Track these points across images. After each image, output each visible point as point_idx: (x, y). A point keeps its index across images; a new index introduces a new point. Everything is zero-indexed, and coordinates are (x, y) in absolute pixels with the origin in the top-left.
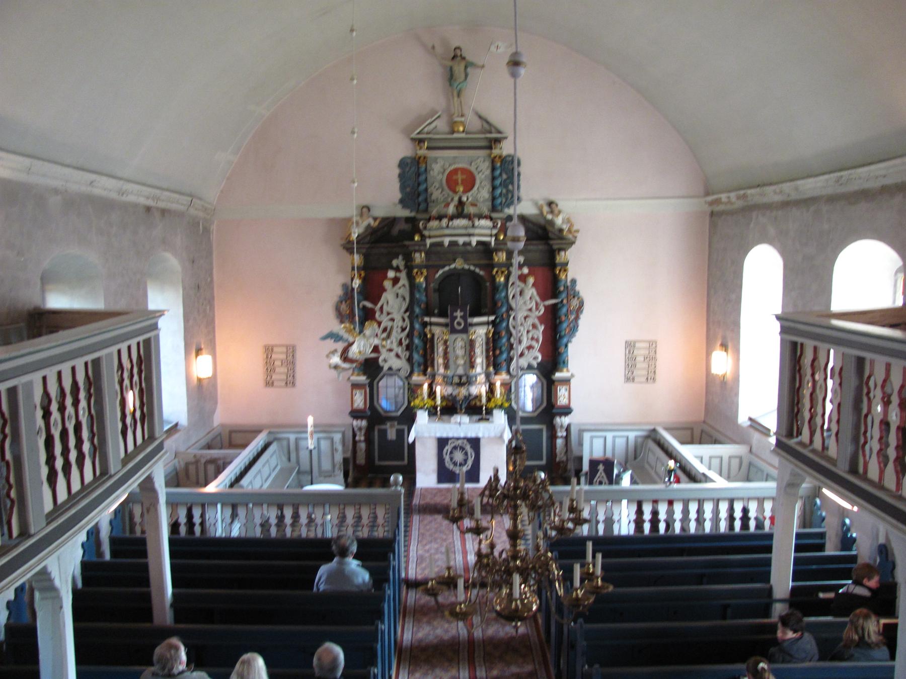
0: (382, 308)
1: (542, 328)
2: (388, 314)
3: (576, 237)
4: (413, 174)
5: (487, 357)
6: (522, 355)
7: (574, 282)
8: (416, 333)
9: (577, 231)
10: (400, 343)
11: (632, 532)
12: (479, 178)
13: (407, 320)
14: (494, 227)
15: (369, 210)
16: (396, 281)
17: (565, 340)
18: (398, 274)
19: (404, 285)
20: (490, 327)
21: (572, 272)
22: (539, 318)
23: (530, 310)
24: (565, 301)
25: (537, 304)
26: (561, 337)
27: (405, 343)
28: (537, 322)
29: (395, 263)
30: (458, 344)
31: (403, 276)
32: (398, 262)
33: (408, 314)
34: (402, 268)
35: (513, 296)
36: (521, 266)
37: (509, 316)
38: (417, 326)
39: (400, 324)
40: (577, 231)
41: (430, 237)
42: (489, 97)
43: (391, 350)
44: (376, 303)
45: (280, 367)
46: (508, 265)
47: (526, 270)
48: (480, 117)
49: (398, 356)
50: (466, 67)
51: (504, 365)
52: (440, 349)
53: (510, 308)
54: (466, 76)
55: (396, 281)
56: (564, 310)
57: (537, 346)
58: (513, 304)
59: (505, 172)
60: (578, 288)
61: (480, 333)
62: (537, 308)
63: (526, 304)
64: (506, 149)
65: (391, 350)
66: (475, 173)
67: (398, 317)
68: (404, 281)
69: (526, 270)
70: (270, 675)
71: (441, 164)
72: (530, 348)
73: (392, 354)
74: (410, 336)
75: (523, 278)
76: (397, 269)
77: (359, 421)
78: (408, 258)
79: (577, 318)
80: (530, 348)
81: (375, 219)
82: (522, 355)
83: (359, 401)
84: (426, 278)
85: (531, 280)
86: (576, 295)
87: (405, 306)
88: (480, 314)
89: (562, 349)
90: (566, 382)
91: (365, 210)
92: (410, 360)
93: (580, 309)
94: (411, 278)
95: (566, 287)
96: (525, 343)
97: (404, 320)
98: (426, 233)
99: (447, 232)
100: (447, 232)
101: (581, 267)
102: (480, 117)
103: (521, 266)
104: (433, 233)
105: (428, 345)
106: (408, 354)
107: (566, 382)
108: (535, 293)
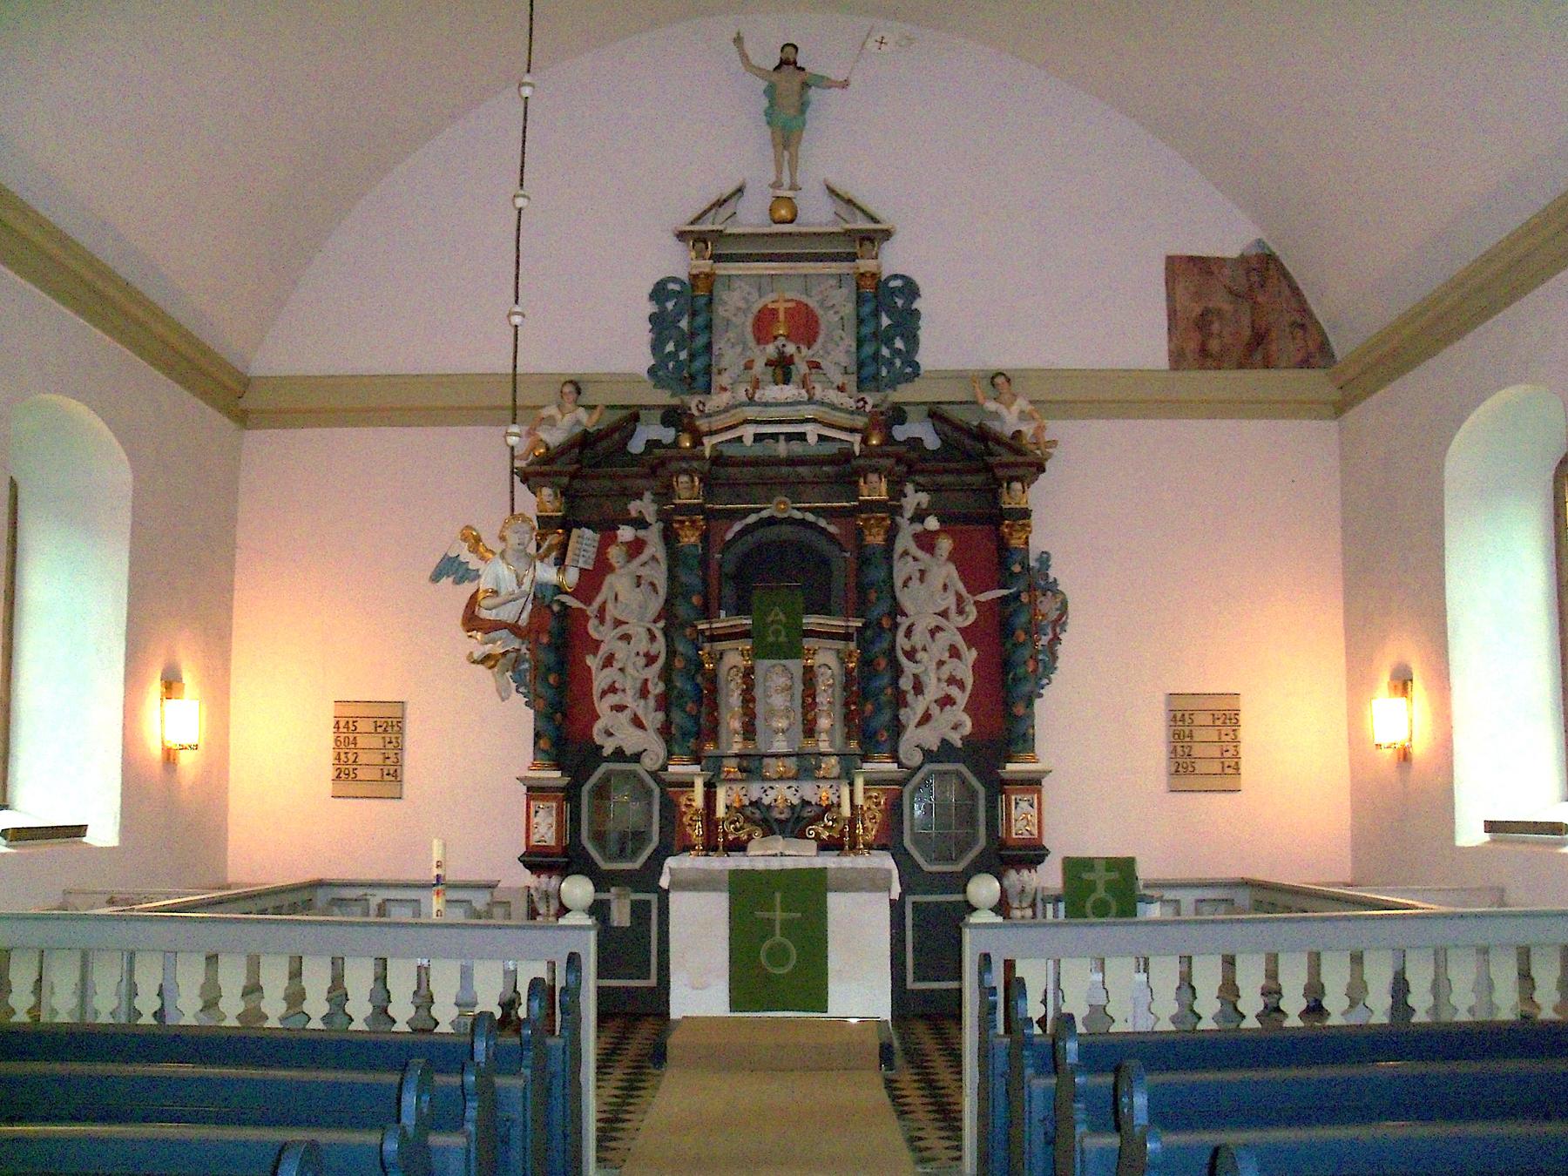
0: (602, 610)
1: (971, 655)
2: (618, 623)
3: (1050, 455)
4: (683, 316)
5: (848, 718)
6: (926, 718)
7: (1045, 559)
8: (679, 663)
9: (1054, 443)
10: (644, 693)
11: (1386, 1020)
12: (827, 320)
13: (659, 634)
14: (859, 411)
15: (579, 392)
16: (636, 547)
17: (1025, 688)
18: (642, 533)
19: (654, 558)
20: (852, 645)
21: (1039, 539)
22: (963, 631)
23: (944, 614)
24: (1024, 598)
25: (960, 599)
26: (1017, 680)
27: (657, 688)
28: (959, 641)
29: (634, 507)
30: (778, 685)
31: (653, 536)
32: (645, 506)
33: (661, 624)
34: (650, 519)
35: (905, 585)
36: (919, 517)
37: (896, 626)
38: (681, 647)
39: (642, 644)
40: (1054, 443)
41: (711, 433)
42: (858, 155)
43: (620, 708)
44: (588, 602)
45: (370, 749)
46: (892, 509)
47: (932, 523)
48: (832, 192)
49: (637, 723)
50: (805, 85)
51: (884, 736)
52: (732, 698)
53: (896, 610)
54: (803, 106)
55: (636, 547)
56: (1023, 619)
57: (962, 698)
58: (904, 598)
59: (889, 310)
60: (1053, 573)
61: (827, 660)
62: (961, 612)
63: (932, 594)
64: (892, 261)
65: (620, 708)
66: (819, 312)
67: (638, 630)
68: (655, 546)
69: (932, 523)
70: (1565, 1116)
71: (741, 295)
72: (946, 701)
73: (624, 717)
74: (666, 675)
75: (926, 542)
76: (640, 523)
77: (544, 878)
78: (666, 493)
79: (1056, 639)
80: (946, 701)
81: (591, 408)
82: (926, 718)
83: (546, 830)
84: (705, 537)
85: (945, 545)
86: (1051, 588)
87: (656, 604)
88: (825, 610)
89: (1020, 709)
90: (1032, 783)
91: (568, 389)
92: (665, 731)
93: (1060, 622)
94: (669, 537)
95: (1026, 568)
96: (933, 690)
97: (653, 638)
98: (703, 425)
99: (750, 412)
100: (750, 412)
101: (1062, 520)
102: (832, 192)
103: (919, 517)
104: (717, 422)
105: (708, 694)
106: (660, 716)
107: (1032, 783)
108: (955, 574)
